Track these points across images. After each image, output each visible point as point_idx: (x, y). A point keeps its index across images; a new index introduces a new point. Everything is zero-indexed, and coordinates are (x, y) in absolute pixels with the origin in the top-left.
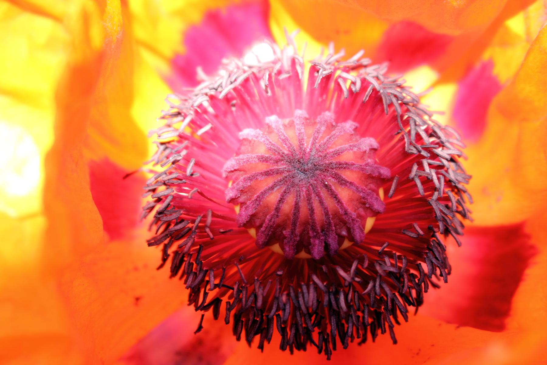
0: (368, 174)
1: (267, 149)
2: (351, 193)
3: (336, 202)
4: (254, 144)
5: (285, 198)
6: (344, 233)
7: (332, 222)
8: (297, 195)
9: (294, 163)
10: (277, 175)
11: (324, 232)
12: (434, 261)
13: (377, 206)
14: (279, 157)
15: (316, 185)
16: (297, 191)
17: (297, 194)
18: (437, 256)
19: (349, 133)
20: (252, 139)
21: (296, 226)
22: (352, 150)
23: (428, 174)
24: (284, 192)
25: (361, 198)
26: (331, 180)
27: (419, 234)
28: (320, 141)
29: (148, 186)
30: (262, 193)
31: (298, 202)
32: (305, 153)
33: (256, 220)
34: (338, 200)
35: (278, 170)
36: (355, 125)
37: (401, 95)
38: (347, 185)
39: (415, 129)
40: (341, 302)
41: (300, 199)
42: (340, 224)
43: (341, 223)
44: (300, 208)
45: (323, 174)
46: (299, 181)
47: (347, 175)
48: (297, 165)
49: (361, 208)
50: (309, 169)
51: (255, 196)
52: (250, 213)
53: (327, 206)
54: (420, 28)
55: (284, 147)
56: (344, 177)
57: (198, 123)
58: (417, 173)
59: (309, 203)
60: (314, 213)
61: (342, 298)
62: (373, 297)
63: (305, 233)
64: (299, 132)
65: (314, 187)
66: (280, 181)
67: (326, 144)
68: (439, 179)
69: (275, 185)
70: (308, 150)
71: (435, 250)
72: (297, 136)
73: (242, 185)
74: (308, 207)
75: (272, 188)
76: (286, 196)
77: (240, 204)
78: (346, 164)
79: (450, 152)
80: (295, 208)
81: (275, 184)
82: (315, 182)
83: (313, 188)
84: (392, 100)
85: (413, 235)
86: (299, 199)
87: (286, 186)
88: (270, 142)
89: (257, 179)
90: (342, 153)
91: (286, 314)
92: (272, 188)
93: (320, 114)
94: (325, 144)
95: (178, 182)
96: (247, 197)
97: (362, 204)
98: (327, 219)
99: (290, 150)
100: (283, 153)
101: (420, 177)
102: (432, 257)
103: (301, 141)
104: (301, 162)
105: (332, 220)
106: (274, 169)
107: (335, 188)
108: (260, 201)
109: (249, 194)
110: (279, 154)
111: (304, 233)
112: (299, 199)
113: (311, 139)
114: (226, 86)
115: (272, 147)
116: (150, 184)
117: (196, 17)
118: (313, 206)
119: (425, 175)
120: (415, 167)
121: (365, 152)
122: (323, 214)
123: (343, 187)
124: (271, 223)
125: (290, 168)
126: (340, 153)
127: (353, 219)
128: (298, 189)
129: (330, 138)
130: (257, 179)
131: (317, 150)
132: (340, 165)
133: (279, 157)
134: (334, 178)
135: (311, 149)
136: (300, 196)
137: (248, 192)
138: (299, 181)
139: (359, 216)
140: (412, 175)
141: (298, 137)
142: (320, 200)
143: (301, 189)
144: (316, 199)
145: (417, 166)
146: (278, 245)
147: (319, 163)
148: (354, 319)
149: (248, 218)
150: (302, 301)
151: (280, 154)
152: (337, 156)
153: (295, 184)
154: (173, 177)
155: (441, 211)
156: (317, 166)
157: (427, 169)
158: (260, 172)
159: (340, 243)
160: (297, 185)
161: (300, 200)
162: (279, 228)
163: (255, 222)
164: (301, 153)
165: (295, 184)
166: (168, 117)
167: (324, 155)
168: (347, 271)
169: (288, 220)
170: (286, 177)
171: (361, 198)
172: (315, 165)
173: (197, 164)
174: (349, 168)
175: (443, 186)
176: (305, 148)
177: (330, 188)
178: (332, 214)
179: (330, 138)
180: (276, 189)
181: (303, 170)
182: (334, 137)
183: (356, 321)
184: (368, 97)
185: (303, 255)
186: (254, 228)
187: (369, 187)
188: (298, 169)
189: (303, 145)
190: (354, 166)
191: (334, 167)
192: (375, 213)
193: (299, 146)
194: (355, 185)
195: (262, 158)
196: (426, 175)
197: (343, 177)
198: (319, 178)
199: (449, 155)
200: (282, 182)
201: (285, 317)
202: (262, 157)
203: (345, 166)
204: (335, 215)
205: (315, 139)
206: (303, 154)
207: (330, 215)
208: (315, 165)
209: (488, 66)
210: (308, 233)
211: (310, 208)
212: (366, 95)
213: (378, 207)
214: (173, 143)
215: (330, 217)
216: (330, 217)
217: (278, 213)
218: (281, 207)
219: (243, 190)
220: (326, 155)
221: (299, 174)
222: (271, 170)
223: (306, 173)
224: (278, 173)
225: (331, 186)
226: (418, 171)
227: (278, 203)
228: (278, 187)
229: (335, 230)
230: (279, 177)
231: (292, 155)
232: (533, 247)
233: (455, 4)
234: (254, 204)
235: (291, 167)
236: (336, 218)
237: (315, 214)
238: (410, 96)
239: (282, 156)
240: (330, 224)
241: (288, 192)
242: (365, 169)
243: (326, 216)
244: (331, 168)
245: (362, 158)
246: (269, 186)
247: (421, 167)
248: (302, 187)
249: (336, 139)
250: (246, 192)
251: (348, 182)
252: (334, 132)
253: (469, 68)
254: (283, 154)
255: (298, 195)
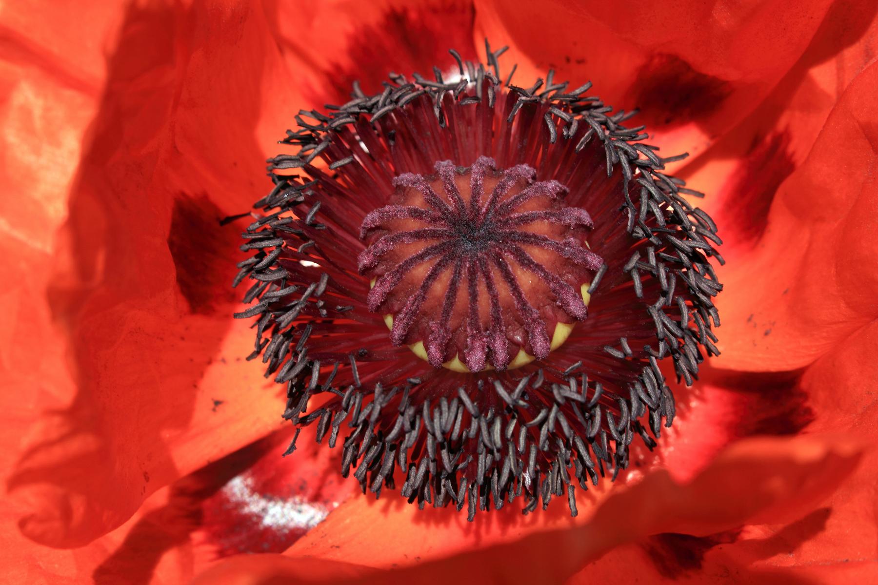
0: (566, 257)
1: (425, 201)
2: (536, 280)
3: (511, 289)
4: (408, 192)
5: (438, 274)
6: (519, 338)
7: (502, 317)
8: (455, 272)
9: (459, 225)
10: (433, 239)
11: (488, 332)
12: (643, 396)
13: (573, 307)
14: (440, 214)
15: (485, 261)
16: (457, 265)
17: (456, 270)
18: (649, 390)
19: (549, 196)
20: (408, 186)
21: (448, 317)
22: (548, 219)
23: (652, 267)
24: (437, 264)
25: (550, 291)
26: (509, 257)
27: (626, 355)
28: (503, 199)
29: (250, 233)
30: (406, 262)
31: (456, 282)
32: (479, 214)
33: (394, 302)
34: (514, 287)
35: (435, 231)
36: (561, 188)
37: (634, 151)
38: (531, 267)
39: (649, 206)
40: (495, 433)
41: (458, 277)
42: (514, 323)
43: (516, 323)
44: (457, 290)
45: (498, 247)
46: (463, 252)
47: (536, 254)
48: (464, 229)
49: (548, 306)
50: (479, 237)
51: (397, 265)
52: (386, 289)
53: (497, 293)
54: (688, 67)
55: (450, 201)
56: (528, 255)
57: (336, 155)
58: (637, 264)
59: (472, 285)
60: (477, 301)
61: (498, 426)
62: (544, 436)
63: (462, 329)
64: (474, 183)
65: (482, 263)
66: (436, 248)
67: (511, 205)
68: (668, 279)
69: (427, 254)
70: (484, 210)
71: (647, 381)
72: (471, 188)
73: (382, 249)
74: (469, 291)
75: (421, 257)
76: (440, 271)
77: (376, 277)
78: (535, 236)
79: (693, 244)
80: (450, 289)
81: (427, 252)
82: (485, 257)
83: (481, 264)
84: (619, 158)
85: (618, 354)
86: (457, 277)
87: (442, 256)
88: (431, 192)
89: (403, 241)
90: (531, 221)
91: (411, 439)
92: (421, 257)
93: (513, 165)
94: (509, 205)
95: (290, 230)
96: (387, 267)
97: (551, 300)
98: (494, 312)
99: (457, 206)
100: (447, 209)
101: (639, 270)
102: (641, 390)
103: (475, 195)
104: (470, 226)
105: (503, 316)
106: (429, 230)
107: (512, 269)
108: (402, 273)
109: (391, 263)
110: (440, 209)
111: (460, 329)
112: (457, 277)
113: (491, 196)
114: (384, 105)
115: (432, 198)
116: (252, 231)
117: (373, 17)
118: (476, 290)
119: (647, 268)
120: (636, 258)
121: (569, 226)
122: (489, 304)
123: (525, 270)
124: (414, 307)
125: (453, 232)
126: (529, 220)
127: (533, 319)
128: (459, 263)
129: (518, 198)
130: (403, 241)
131: (496, 211)
132: (526, 237)
133: (440, 214)
134: (513, 254)
135: (488, 210)
136: (459, 273)
137: (388, 261)
138: (463, 252)
139: (543, 317)
140: (628, 266)
141: (473, 190)
142: (487, 284)
143: (463, 263)
144: (483, 281)
145: (639, 256)
146: (423, 345)
147: (495, 231)
148: (512, 464)
149: (383, 296)
150: (438, 423)
151: (442, 210)
152: (523, 224)
153: (456, 255)
154: (285, 222)
155: (664, 325)
156: (491, 234)
157: (652, 262)
158: (408, 231)
159: (512, 356)
160: (459, 257)
161: (459, 279)
162: (426, 318)
163: (393, 305)
164: (472, 212)
165: (456, 255)
166: (295, 141)
167: (505, 220)
168: (510, 391)
169: (438, 307)
170: (444, 244)
171: (550, 291)
172: (489, 233)
173: (323, 211)
174: (538, 244)
175: (672, 291)
176: (479, 207)
177: (506, 267)
178: (503, 307)
179: (519, 197)
180: (427, 259)
181: (472, 238)
182: (524, 197)
183: (515, 467)
184: (584, 145)
185: (456, 364)
186: (391, 314)
187: (565, 278)
188: (465, 235)
189: (477, 201)
190: (546, 242)
191: (516, 239)
192: (571, 319)
193: (471, 203)
194: (543, 270)
195: (415, 213)
196: (649, 268)
197: (526, 255)
198: (492, 251)
199: (691, 247)
200: (437, 250)
201: (409, 442)
202: (416, 211)
203: (532, 239)
204: (509, 308)
205: (496, 196)
206: (476, 215)
207: (499, 307)
208: (489, 233)
209: (784, 138)
210: (466, 331)
211: (472, 292)
212: (581, 142)
213: (577, 309)
214: (296, 179)
215: (499, 311)
216: (499, 311)
217: (425, 293)
218: (431, 285)
219: (382, 256)
220: (508, 221)
221: (464, 243)
222: (425, 231)
223: (475, 242)
224: (434, 237)
225: (507, 265)
226: (640, 262)
227: (427, 279)
228: (430, 256)
229: (506, 331)
230: (435, 243)
231: (459, 214)
232: (809, 411)
233: (724, 23)
234: (393, 277)
235: (455, 231)
236: (509, 314)
237: (478, 303)
238: (647, 156)
239: (445, 214)
240: (498, 320)
241: (444, 266)
242: (563, 250)
243: (493, 307)
244: (512, 240)
245: (563, 235)
246: (418, 253)
247: (645, 257)
248: (465, 261)
249: (527, 200)
250: (386, 260)
251: (533, 263)
252: (525, 191)
253: (756, 141)
254: (445, 210)
255: (458, 271)
